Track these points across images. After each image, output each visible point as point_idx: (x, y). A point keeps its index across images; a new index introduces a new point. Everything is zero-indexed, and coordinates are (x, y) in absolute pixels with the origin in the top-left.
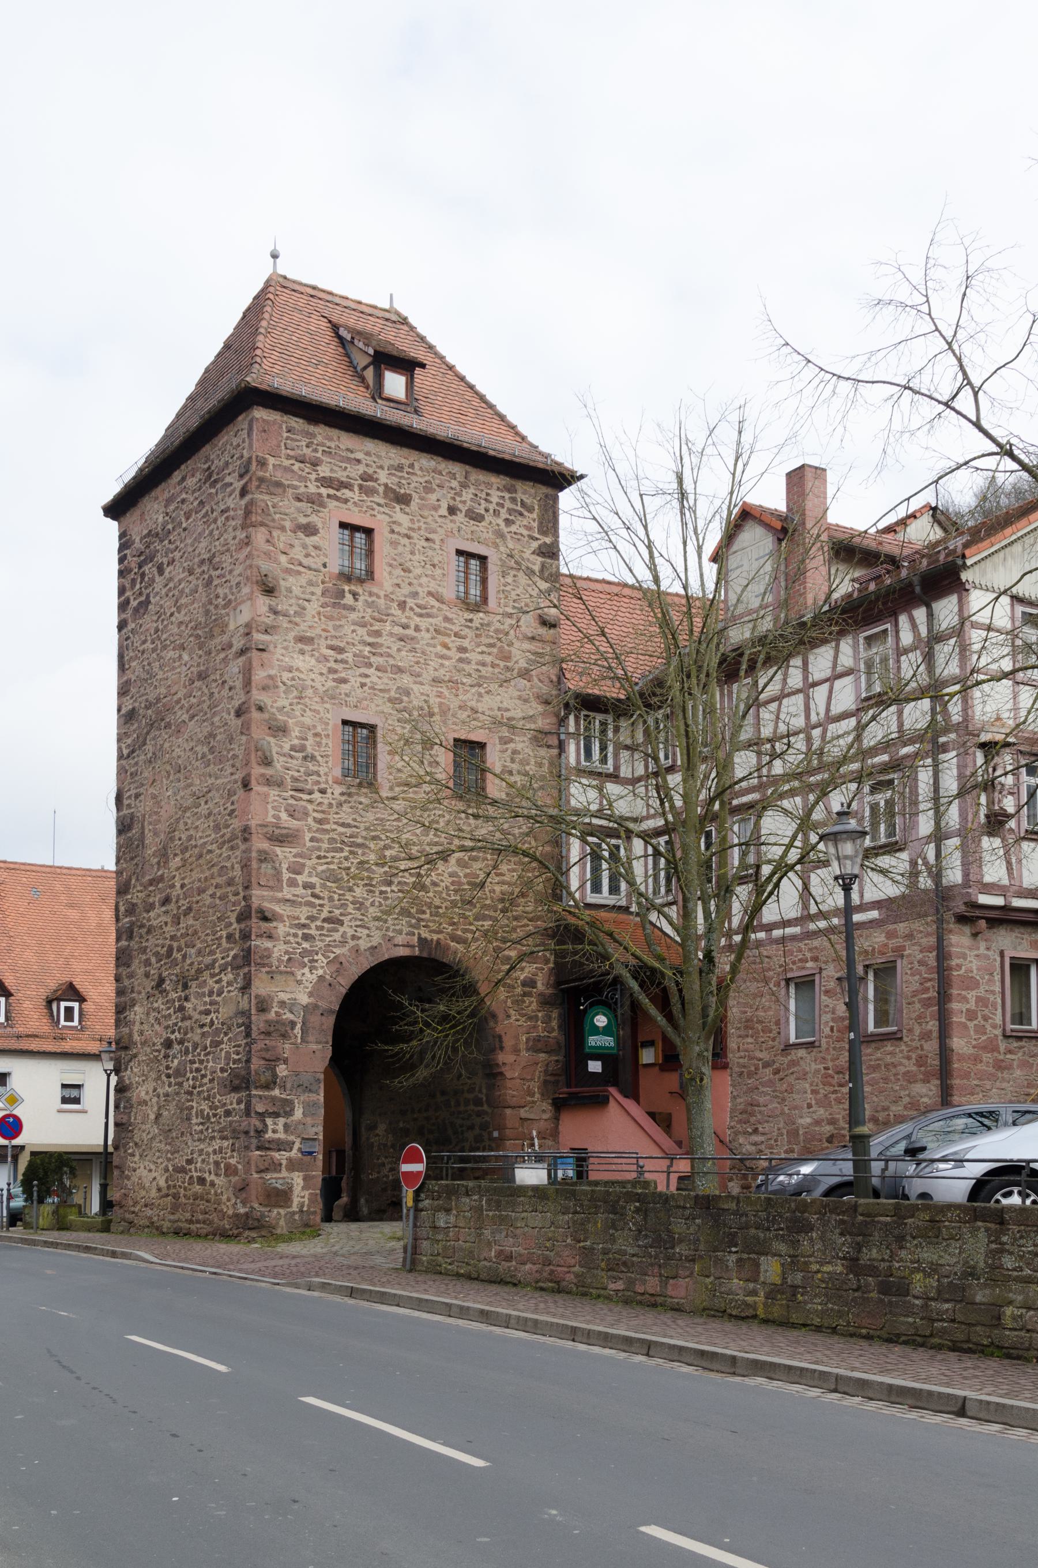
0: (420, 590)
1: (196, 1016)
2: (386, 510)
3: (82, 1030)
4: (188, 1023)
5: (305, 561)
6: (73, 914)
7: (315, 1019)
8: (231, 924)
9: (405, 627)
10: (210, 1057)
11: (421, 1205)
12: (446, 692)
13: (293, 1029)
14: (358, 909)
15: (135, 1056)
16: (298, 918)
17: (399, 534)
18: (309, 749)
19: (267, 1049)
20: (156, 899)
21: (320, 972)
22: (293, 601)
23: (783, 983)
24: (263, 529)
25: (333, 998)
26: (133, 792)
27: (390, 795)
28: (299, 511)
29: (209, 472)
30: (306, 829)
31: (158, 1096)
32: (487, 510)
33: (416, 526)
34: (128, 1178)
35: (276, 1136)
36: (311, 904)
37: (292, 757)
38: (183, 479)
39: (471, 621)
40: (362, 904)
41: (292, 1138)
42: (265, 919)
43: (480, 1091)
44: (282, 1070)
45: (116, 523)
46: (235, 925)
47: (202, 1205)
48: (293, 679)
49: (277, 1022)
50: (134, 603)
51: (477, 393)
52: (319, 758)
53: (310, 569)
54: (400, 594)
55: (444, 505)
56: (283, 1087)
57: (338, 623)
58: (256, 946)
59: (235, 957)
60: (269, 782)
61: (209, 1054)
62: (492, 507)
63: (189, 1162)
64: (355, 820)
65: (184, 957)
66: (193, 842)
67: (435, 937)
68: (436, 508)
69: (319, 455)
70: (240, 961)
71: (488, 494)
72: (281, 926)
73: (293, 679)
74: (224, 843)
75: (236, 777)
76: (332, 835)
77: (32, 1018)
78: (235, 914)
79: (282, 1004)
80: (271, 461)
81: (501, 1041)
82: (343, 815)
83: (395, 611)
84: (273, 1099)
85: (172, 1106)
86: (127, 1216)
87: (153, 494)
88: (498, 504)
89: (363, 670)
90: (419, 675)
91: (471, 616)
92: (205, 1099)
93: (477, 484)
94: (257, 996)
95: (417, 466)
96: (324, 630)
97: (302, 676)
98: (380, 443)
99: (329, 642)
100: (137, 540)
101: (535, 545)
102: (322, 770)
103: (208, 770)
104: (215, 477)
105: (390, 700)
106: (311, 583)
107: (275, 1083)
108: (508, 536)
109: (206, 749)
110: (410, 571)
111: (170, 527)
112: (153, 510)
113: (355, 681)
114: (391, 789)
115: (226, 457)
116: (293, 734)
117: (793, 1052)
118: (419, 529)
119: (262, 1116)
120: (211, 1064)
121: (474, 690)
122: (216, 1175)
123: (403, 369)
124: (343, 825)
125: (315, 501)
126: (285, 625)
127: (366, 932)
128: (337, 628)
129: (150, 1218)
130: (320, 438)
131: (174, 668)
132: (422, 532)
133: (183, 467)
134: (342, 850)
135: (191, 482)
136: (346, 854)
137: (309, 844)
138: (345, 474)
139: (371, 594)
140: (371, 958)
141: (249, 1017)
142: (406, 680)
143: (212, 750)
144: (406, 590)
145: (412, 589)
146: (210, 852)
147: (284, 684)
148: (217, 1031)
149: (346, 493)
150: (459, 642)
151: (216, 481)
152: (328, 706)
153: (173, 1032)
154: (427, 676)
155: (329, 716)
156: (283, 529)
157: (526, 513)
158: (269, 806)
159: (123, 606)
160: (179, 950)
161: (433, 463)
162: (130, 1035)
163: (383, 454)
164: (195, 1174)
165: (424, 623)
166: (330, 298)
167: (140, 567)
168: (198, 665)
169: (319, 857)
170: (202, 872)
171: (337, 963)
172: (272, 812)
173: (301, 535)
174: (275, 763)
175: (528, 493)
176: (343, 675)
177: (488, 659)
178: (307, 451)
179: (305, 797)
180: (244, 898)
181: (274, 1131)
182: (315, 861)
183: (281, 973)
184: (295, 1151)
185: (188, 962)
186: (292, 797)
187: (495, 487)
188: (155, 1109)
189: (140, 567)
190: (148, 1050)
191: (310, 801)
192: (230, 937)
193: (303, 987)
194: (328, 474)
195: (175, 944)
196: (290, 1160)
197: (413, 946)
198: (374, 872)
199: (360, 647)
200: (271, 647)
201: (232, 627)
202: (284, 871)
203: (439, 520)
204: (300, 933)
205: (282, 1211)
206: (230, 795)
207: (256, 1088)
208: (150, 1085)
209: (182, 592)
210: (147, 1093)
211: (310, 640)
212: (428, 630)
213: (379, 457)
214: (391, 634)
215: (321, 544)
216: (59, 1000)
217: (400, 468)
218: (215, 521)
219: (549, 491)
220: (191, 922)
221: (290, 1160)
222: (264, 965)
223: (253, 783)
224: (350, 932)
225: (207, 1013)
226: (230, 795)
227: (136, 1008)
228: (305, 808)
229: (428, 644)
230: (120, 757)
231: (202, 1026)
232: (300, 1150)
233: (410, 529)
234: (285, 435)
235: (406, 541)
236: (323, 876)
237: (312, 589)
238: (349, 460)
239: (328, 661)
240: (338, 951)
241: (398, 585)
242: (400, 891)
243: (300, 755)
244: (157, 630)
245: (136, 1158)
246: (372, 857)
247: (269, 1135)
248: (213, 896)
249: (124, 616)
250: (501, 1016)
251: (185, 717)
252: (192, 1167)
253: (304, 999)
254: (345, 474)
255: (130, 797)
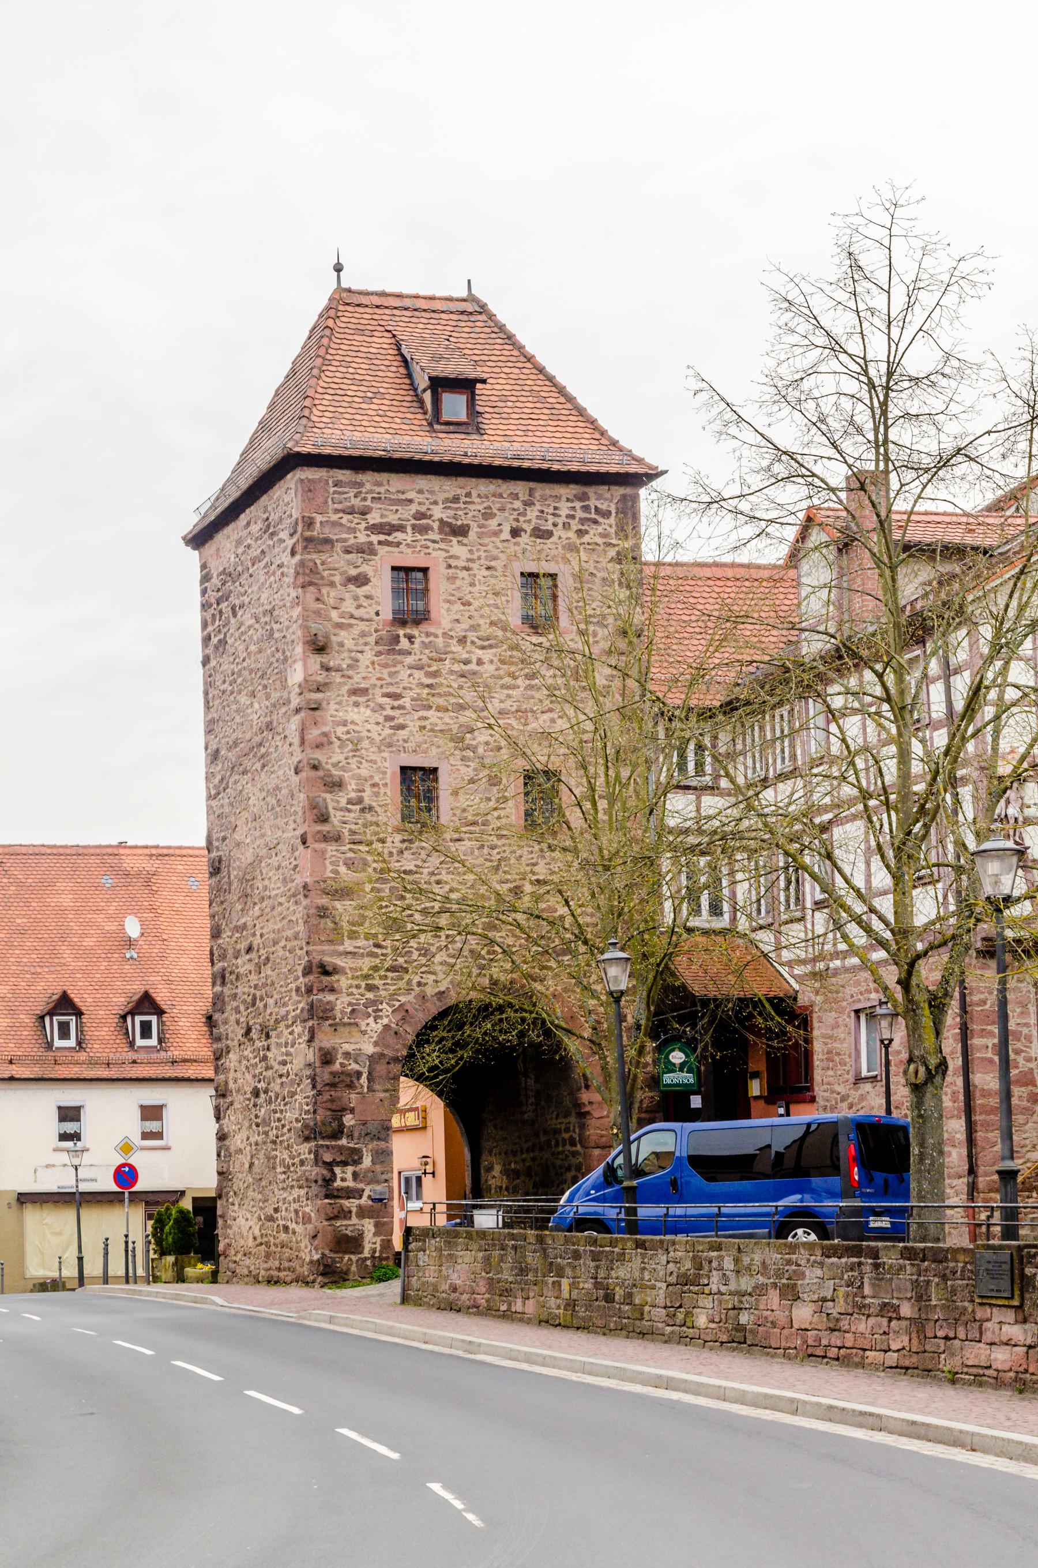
0: (482, 622)
1: (276, 1066)
2: (442, 546)
4: (270, 1073)
5: (357, 613)
13: (358, 1079)
14: (425, 955)
15: (232, 1104)
16: (361, 969)
17: (456, 567)
18: (367, 801)
19: (332, 1100)
20: (243, 946)
21: (385, 1021)
22: (346, 655)
23: (853, 1014)
24: (311, 588)
28: (349, 563)
33: (475, 557)
34: (230, 1227)
35: (345, 1184)
36: (372, 955)
37: (349, 811)
38: (248, 524)
41: (361, 1186)
44: (348, 1120)
46: (301, 979)
48: (348, 733)
50: (215, 640)
52: (378, 809)
53: (362, 620)
54: (459, 630)
55: (506, 529)
56: (351, 1136)
57: (393, 670)
62: (560, 521)
63: (276, 1210)
68: (496, 534)
69: (368, 503)
70: (306, 1015)
71: (556, 508)
72: (343, 979)
73: (348, 733)
79: (347, 1055)
80: (319, 518)
82: (404, 862)
83: (456, 648)
84: (341, 1149)
88: (568, 516)
93: (544, 498)
95: (474, 493)
96: (379, 679)
97: (357, 728)
98: (433, 477)
99: (385, 690)
107: (342, 1132)
109: (274, 802)
110: (469, 604)
113: (413, 726)
116: (349, 788)
117: (862, 1085)
118: (479, 558)
123: (463, 387)
126: (338, 680)
127: (433, 977)
128: (392, 675)
130: (368, 486)
132: (482, 562)
135: (255, 528)
139: (428, 635)
140: (438, 1004)
145: (471, 622)
146: (280, 904)
147: (339, 739)
149: (399, 536)
155: (387, 765)
156: (332, 584)
157: (601, 520)
158: (327, 862)
162: (226, 1083)
163: (436, 489)
164: (281, 1223)
165: (486, 655)
166: (397, 303)
170: (275, 923)
171: (404, 1013)
172: (330, 868)
173: (351, 587)
174: (333, 819)
175: (606, 498)
176: (401, 721)
178: (357, 502)
181: (343, 1180)
183: (345, 1024)
185: (268, 1011)
187: (564, 499)
192: (298, 990)
195: (258, 993)
196: (360, 1207)
200: (324, 704)
205: (354, 1258)
208: (244, 1134)
209: (251, 638)
211: (364, 692)
212: (492, 662)
213: (432, 492)
215: (373, 593)
217: (456, 499)
218: (274, 574)
220: (269, 972)
221: (360, 1207)
222: (327, 1019)
224: (416, 979)
225: (284, 1063)
227: (231, 1055)
228: (364, 859)
229: (493, 676)
231: (281, 1076)
232: (369, 1197)
233: (469, 560)
234: (332, 490)
235: (465, 573)
239: (384, 709)
240: (403, 999)
241: (458, 621)
243: (358, 807)
245: (236, 1207)
247: (338, 1183)
252: (278, 1215)
253: (369, 1049)
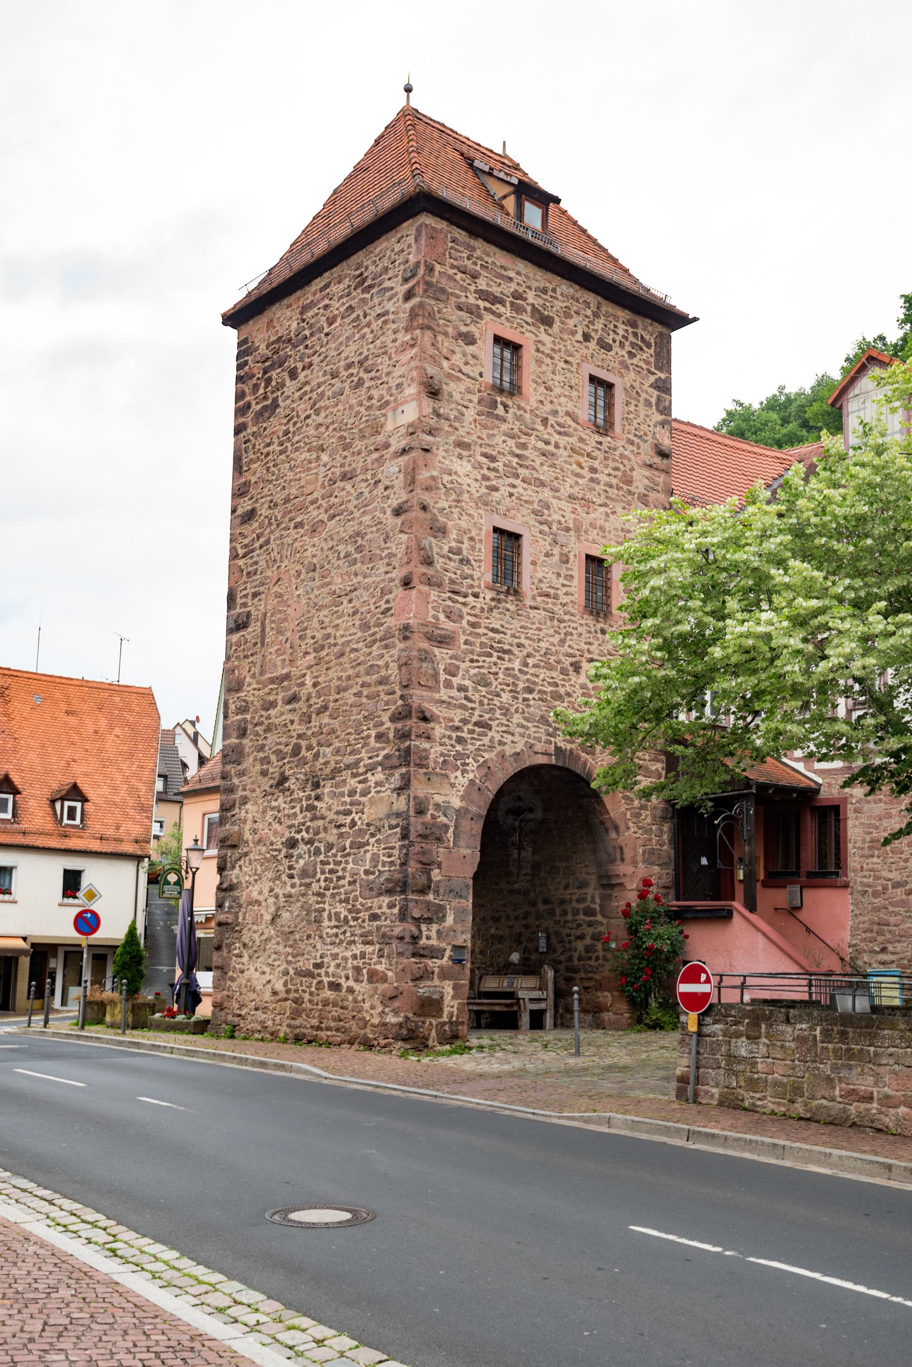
0: (559, 409)
3: (83, 829)
4: (320, 823)
6: (73, 720)
7: (466, 824)
8: (383, 724)
9: (547, 443)
10: (350, 859)
11: (706, 1030)
12: (580, 509)
13: (446, 832)
14: (504, 715)
15: (246, 854)
16: (452, 720)
17: (543, 353)
18: (465, 552)
21: (471, 776)
25: (482, 803)
26: (250, 591)
27: (533, 604)
29: (361, 280)
30: (459, 629)
31: (277, 897)
32: (614, 341)
33: (557, 348)
34: (232, 979)
35: (430, 942)
37: (450, 559)
38: (327, 286)
39: (600, 443)
40: (508, 710)
41: (443, 945)
42: (425, 719)
43: (593, 901)
45: (235, 332)
46: (388, 724)
47: (336, 1012)
49: (433, 825)
51: (589, 237)
53: (469, 377)
56: (437, 892)
57: (491, 432)
58: (417, 747)
59: (386, 757)
60: (429, 582)
61: (349, 854)
62: (618, 338)
63: (318, 966)
64: (502, 626)
65: (317, 756)
66: (332, 641)
67: (569, 746)
68: (573, 333)
69: (478, 268)
71: (615, 326)
72: (437, 727)
74: (375, 641)
75: (393, 575)
76: (483, 639)
77: (37, 816)
78: (389, 713)
79: (437, 806)
80: (438, 268)
81: (622, 853)
84: (428, 903)
85: (296, 908)
86: (230, 1018)
87: (285, 302)
89: (511, 480)
90: (557, 491)
91: (601, 439)
92: (341, 901)
93: (607, 315)
94: (415, 798)
97: (459, 480)
98: (529, 264)
99: (483, 450)
100: (263, 346)
101: (652, 379)
102: (476, 574)
103: (353, 568)
104: (369, 282)
105: (534, 512)
106: (469, 391)
107: (429, 887)
108: (631, 367)
109: (350, 548)
111: (307, 332)
112: (286, 317)
113: (504, 490)
114: (534, 598)
115: (386, 262)
118: (560, 351)
119: (417, 921)
120: (351, 865)
121: (602, 509)
122: (356, 981)
124: (493, 630)
125: (473, 311)
126: (446, 428)
127: (510, 738)
129: (262, 1023)
130: (478, 253)
131: (309, 469)
133: (327, 274)
134: (491, 655)
135: (335, 289)
136: (494, 659)
137: (463, 647)
138: (500, 289)
139: (519, 408)
141: (407, 818)
142: (546, 494)
143: (359, 549)
144: (548, 408)
146: (356, 650)
148: (361, 832)
150: (591, 462)
151: (371, 286)
152: (481, 512)
153: (299, 832)
154: (565, 490)
155: (482, 521)
156: (446, 334)
159: (240, 411)
160: (310, 748)
161: (571, 290)
163: (531, 275)
165: (563, 441)
167: (265, 372)
168: (342, 466)
169: (472, 661)
172: (432, 612)
174: (435, 564)
175: (648, 330)
176: (494, 483)
177: (614, 481)
179: (461, 599)
180: (402, 697)
181: (428, 938)
182: (468, 664)
183: (437, 774)
184: (446, 959)
185: (321, 760)
186: (450, 598)
187: (621, 320)
188: (272, 909)
189: (265, 372)
190: (264, 849)
191: (464, 604)
193: (457, 793)
194: (484, 288)
195: (304, 743)
197: (550, 755)
198: (518, 679)
199: (510, 458)
200: (434, 450)
201: (389, 427)
202: (442, 672)
203: (576, 345)
204: (454, 735)
205: (434, 1022)
206: (383, 592)
207: (413, 892)
208: (266, 886)
210: (260, 893)
212: (565, 449)
213: (528, 278)
214: (535, 449)
216: (63, 799)
217: (545, 291)
218: (368, 325)
219: (664, 330)
221: (441, 968)
223: (415, 581)
224: (497, 737)
225: (348, 813)
226: (383, 592)
227: (248, 806)
228: (460, 610)
229: (565, 462)
230: (234, 556)
231: (339, 827)
232: (450, 958)
234: (450, 244)
235: (548, 361)
236: (475, 679)
237: (470, 396)
238: (502, 277)
239: (482, 468)
240: (487, 756)
241: (541, 402)
242: (540, 699)
243: (457, 557)
244: (287, 433)
245: (245, 959)
246: (517, 665)
247: (423, 941)
248: (358, 695)
249: (242, 420)
250: (622, 827)
251: (324, 517)
252: (322, 971)
253: (457, 803)
254: (500, 289)
255: (246, 596)
